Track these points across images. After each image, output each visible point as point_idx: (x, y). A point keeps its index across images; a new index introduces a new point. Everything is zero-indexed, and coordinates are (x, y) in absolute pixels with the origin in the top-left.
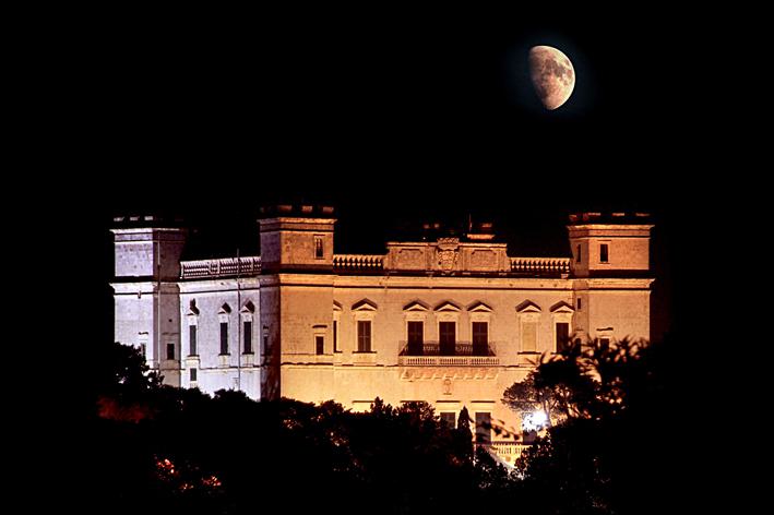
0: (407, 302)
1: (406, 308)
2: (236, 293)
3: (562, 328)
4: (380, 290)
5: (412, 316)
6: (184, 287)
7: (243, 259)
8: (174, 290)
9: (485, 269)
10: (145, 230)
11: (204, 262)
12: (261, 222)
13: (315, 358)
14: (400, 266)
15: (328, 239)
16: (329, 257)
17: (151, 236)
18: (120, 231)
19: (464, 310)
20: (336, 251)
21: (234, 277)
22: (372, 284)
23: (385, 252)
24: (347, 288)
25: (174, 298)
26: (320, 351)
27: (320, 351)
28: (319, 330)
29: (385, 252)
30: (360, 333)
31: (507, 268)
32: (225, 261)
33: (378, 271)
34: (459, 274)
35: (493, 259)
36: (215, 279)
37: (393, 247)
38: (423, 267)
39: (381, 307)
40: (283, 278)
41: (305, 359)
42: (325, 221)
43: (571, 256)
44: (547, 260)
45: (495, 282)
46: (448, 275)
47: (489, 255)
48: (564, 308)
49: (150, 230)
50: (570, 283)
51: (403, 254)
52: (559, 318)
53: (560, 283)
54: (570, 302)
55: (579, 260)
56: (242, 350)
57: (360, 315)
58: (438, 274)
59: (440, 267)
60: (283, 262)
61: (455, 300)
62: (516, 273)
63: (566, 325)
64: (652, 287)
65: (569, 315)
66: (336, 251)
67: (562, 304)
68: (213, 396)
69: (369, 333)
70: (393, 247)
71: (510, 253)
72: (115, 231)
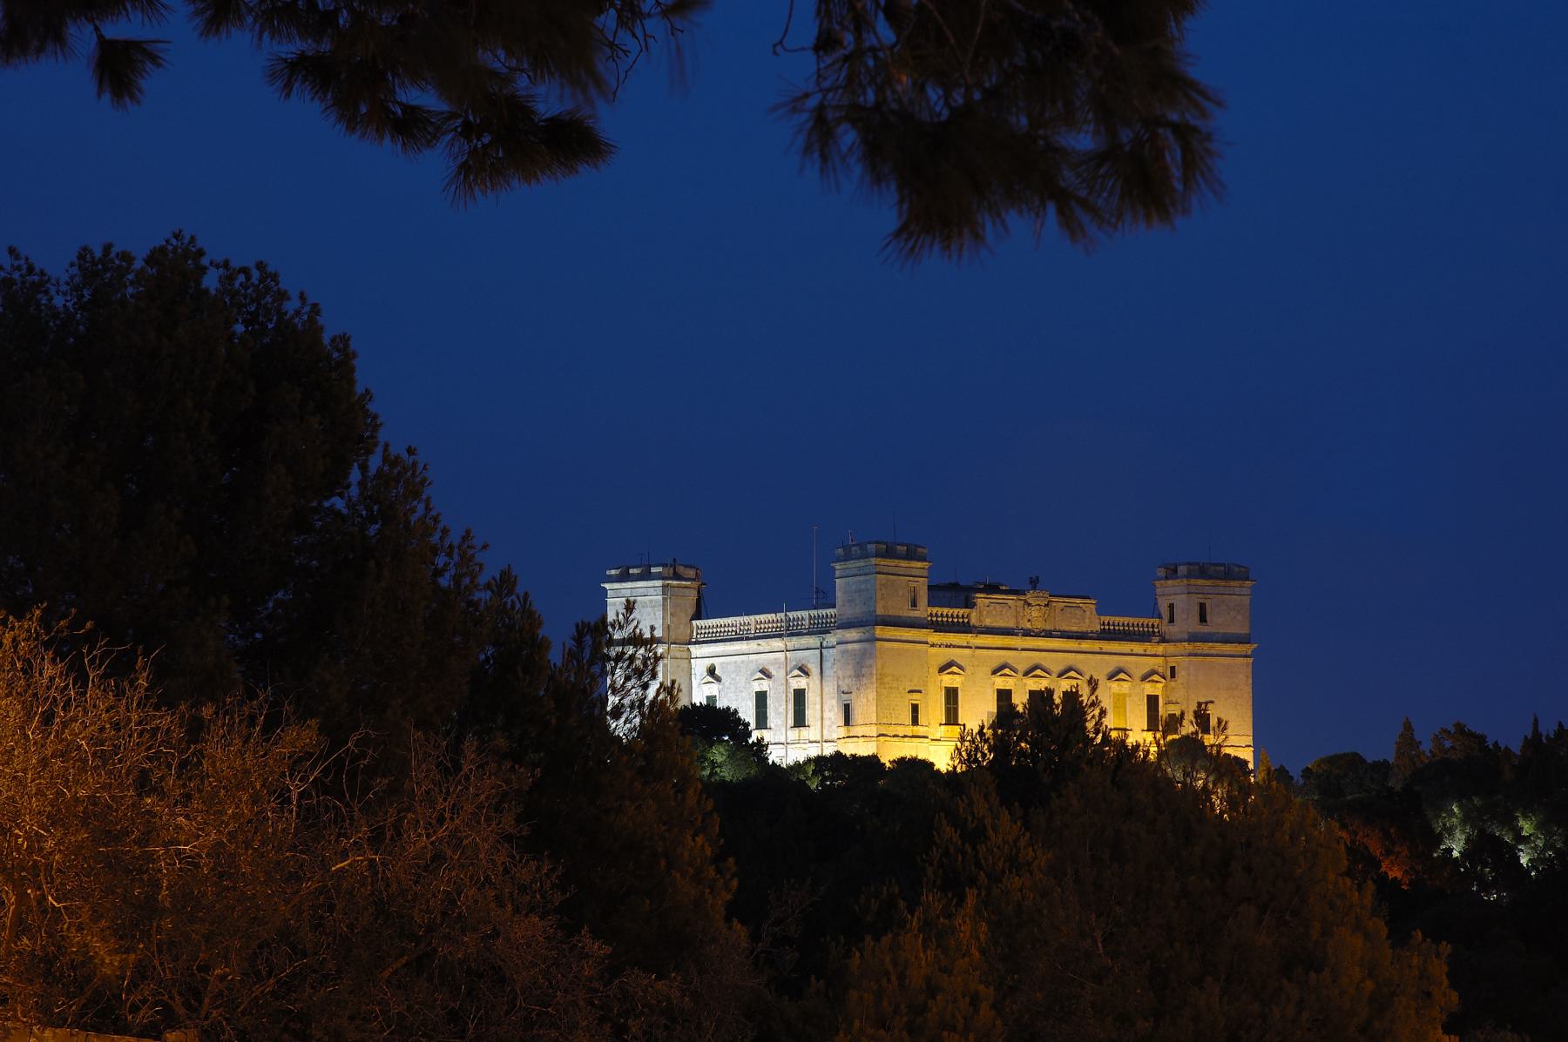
0: (995, 665)
1: (994, 673)
2: (781, 655)
3: (1152, 701)
4: (967, 651)
5: (1001, 683)
6: (696, 650)
7: (791, 615)
8: (685, 655)
9: (1075, 629)
10: (650, 583)
11: (729, 620)
12: (838, 566)
13: (910, 730)
14: (988, 622)
15: (922, 586)
16: (924, 611)
17: (660, 591)
18: (616, 586)
19: (1054, 676)
20: (930, 604)
21: (780, 636)
22: (761, 649)
23: (970, 604)
24: (940, 647)
25: (684, 664)
26: (915, 722)
27: (915, 722)
28: (916, 696)
29: (970, 604)
30: (948, 702)
31: (1098, 628)
32: (763, 617)
33: (964, 628)
34: (1049, 634)
35: (1083, 618)
36: (748, 639)
37: (981, 600)
38: (1011, 624)
39: (969, 669)
40: (879, 631)
41: (901, 731)
42: (919, 564)
43: (1160, 617)
44: (1131, 620)
45: (1085, 645)
46: (1037, 635)
47: (1078, 612)
48: (1156, 677)
49: (659, 583)
50: (1160, 649)
51: (987, 609)
52: (1149, 689)
53: (1150, 648)
54: (1160, 670)
55: (1172, 620)
56: (791, 722)
57: (948, 680)
58: (1027, 633)
59: (1028, 626)
60: (879, 612)
61: (1080, 667)
62: (1107, 635)
63: (1156, 697)
64: (1254, 654)
65: (1160, 686)
66: (930, 604)
67: (1153, 672)
68: (1516, 748)
69: (956, 702)
70: (981, 600)
71: (1100, 612)
72: (607, 586)
